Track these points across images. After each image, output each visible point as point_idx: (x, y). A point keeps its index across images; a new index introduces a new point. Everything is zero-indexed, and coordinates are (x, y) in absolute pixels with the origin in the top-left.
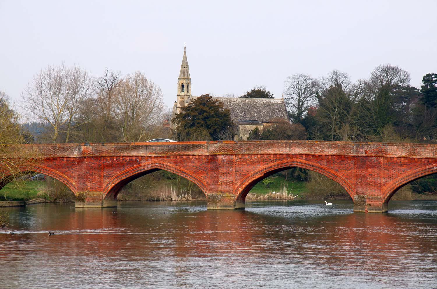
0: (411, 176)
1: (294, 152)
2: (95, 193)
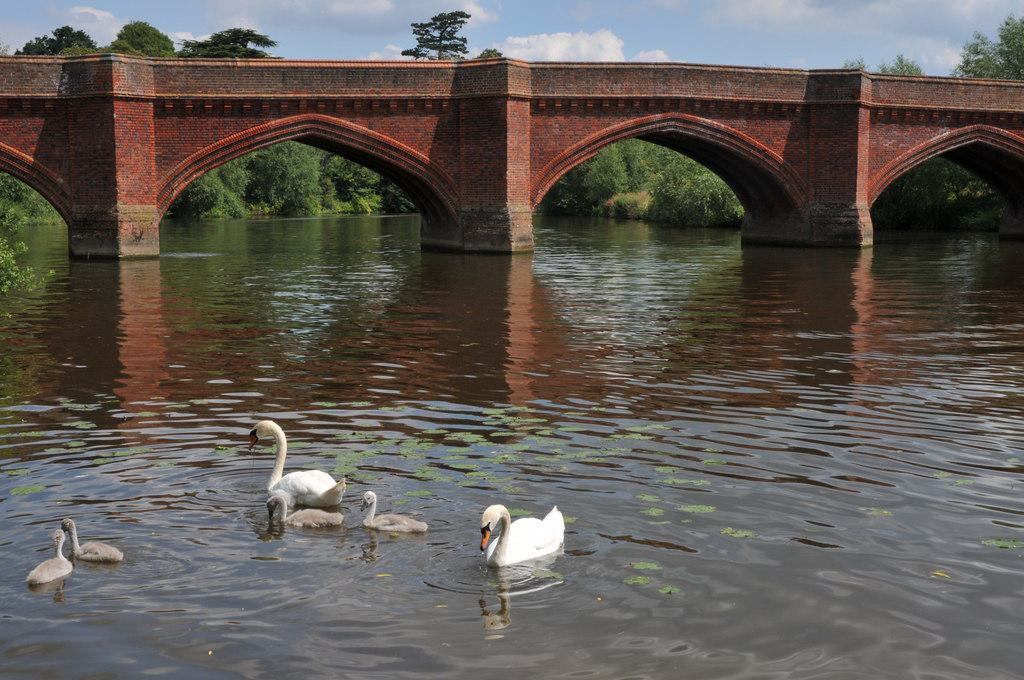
0: (921, 155)
1: (676, 94)
2: (138, 207)
